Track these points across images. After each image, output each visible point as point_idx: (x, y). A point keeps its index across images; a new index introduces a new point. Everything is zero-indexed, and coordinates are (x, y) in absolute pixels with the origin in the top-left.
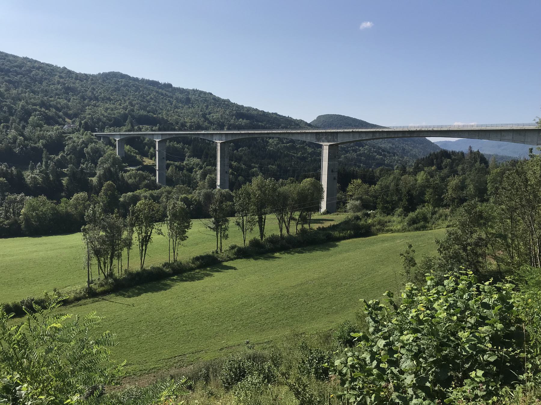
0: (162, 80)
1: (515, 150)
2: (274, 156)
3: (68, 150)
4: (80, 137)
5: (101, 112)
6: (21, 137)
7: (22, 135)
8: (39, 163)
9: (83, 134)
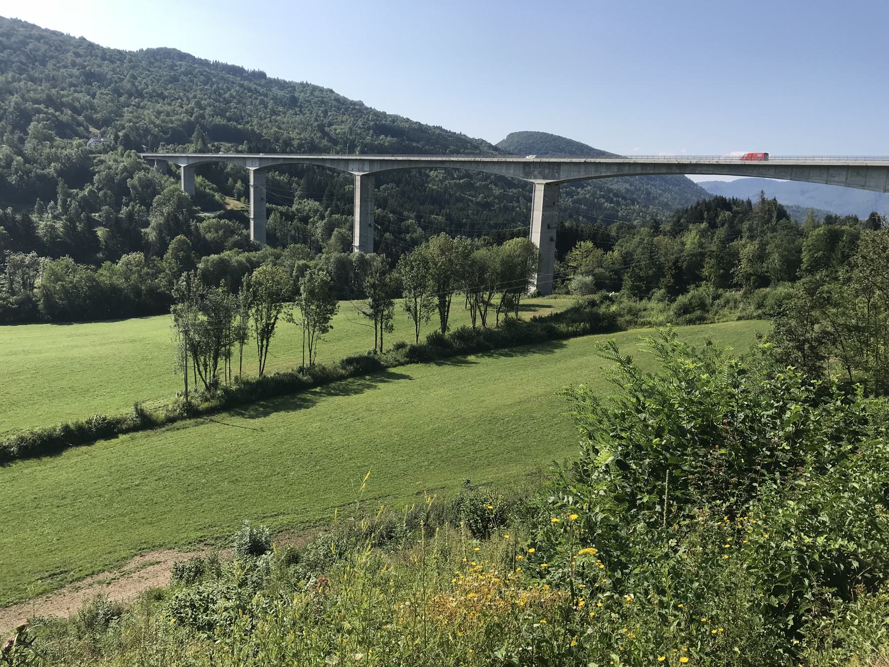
0: (250, 65)
1: (855, 203)
2: (438, 200)
3: (99, 181)
4: (120, 159)
5: (150, 118)
6: (19, 158)
7: (20, 153)
8: (52, 202)
9: (122, 155)
